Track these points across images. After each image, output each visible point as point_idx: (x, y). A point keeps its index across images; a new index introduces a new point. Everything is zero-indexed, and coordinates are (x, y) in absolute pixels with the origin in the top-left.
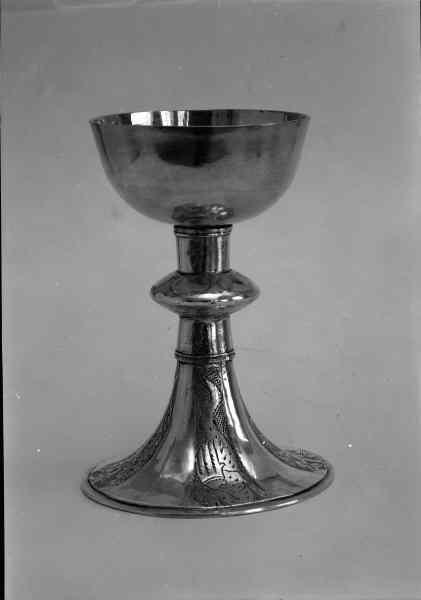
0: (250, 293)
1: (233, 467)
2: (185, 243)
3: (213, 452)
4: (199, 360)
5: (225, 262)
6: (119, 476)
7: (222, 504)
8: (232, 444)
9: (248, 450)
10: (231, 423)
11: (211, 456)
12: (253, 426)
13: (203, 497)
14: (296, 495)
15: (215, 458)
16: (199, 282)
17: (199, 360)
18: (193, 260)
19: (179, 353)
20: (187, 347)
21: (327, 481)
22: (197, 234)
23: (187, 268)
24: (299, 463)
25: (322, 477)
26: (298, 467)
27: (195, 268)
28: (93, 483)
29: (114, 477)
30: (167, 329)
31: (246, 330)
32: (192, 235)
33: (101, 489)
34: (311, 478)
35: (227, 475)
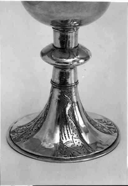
0: (87, 58)
1: (77, 136)
2: (58, 35)
3: (68, 129)
4: (63, 85)
5: (76, 41)
6: (25, 136)
7: (73, 156)
8: (79, 130)
9: (86, 132)
10: (77, 120)
11: (67, 131)
12: (85, 113)
13: (62, 154)
14: (106, 150)
15: (69, 131)
16: (64, 52)
17: (63, 85)
18: (81, 135)
19: (53, 82)
20: (57, 81)
21: (118, 141)
22: (64, 31)
23: (58, 45)
24: (104, 129)
25: (115, 138)
26: (105, 132)
27: (81, 134)
28: (13, 139)
29: (22, 136)
30: (47, 72)
31: (83, 75)
32: (61, 31)
33: (17, 143)
34: (110, 139)
35: (75, 140)
